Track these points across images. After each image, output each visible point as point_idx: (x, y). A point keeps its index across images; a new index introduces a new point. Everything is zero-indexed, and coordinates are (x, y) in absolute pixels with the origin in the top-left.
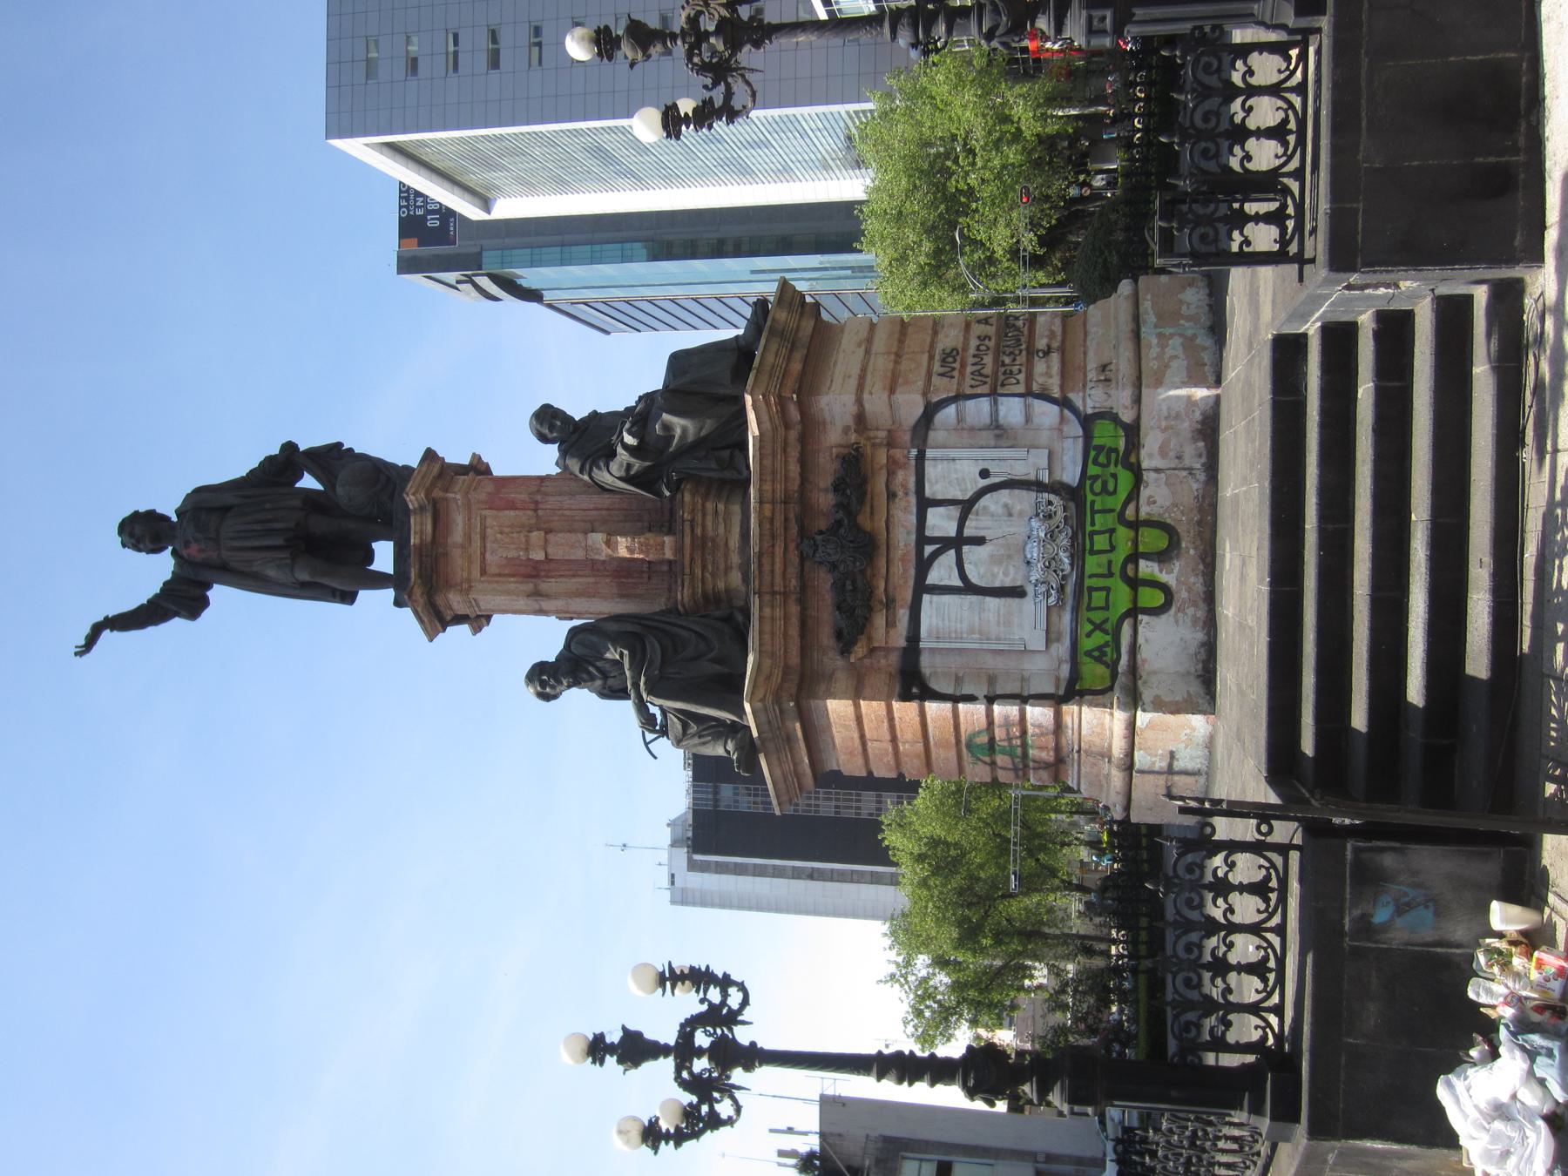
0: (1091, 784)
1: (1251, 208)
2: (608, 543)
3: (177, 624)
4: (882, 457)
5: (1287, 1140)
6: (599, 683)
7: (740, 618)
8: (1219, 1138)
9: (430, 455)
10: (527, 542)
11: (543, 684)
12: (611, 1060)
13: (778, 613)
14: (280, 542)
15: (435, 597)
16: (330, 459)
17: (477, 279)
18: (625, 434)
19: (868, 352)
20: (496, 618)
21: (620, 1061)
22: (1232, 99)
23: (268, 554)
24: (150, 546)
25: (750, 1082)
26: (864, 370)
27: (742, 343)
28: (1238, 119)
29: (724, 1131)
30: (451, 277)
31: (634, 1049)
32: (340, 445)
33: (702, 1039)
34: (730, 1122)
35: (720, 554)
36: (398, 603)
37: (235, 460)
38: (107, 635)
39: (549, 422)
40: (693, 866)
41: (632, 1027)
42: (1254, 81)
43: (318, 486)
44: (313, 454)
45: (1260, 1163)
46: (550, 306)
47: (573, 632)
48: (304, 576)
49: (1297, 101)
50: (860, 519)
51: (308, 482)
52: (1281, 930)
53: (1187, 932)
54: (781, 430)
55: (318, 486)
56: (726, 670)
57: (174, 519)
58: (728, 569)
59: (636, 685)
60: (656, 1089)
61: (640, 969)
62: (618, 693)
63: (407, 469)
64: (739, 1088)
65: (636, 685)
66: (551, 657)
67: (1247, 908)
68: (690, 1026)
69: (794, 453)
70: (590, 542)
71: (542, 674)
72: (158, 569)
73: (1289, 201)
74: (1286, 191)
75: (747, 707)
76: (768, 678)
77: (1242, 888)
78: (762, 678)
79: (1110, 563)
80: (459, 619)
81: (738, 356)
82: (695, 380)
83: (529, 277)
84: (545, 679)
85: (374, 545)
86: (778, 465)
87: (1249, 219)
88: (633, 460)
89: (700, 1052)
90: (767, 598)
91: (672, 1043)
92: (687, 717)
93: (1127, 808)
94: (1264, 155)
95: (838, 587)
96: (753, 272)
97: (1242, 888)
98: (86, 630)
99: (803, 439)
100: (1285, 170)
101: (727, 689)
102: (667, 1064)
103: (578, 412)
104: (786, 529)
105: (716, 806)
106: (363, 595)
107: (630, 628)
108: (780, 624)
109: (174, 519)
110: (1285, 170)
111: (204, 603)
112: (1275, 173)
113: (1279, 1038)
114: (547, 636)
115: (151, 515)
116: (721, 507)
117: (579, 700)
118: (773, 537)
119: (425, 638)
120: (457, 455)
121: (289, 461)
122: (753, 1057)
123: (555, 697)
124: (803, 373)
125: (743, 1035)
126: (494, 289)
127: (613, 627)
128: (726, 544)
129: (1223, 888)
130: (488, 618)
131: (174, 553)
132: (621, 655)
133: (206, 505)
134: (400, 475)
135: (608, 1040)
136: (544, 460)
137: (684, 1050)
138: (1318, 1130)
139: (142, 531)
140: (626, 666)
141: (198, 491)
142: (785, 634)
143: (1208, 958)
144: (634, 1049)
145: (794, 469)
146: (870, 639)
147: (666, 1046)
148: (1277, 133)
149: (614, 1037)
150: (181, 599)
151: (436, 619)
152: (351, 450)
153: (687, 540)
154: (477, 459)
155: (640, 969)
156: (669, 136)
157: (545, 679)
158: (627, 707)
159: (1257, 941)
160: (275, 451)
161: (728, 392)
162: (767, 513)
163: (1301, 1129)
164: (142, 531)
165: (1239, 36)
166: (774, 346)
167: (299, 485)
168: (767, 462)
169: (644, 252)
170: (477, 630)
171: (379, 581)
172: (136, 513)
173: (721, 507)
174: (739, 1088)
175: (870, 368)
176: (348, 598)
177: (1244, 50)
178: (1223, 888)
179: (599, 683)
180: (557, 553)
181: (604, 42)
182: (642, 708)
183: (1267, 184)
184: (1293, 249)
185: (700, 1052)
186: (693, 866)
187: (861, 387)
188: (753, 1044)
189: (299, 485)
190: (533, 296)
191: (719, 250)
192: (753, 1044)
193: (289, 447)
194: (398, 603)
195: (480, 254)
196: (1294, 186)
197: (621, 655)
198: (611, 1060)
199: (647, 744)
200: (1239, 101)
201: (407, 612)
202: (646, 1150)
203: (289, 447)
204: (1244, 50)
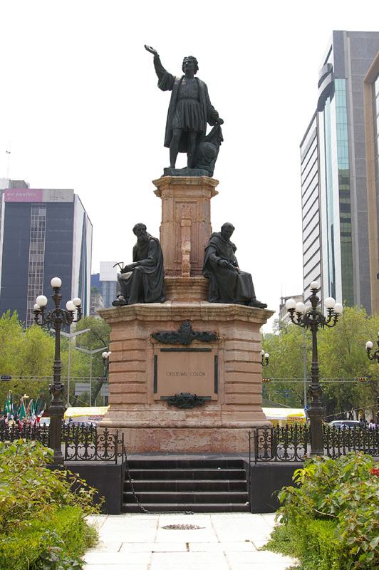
3: (156, 79)
6: (140, 248)
15: (167, 185)
16: (217, 137)
17: (330, 75)
19: (249, 341)
23: (183, 120)
26: (243, 340)
30: (331, 61)
32: (223, 141)
35: (185, 291)
36: (165, 169)
37: (217, 100)
38: (153, 56)
39: (228, 230)
43: (207, 134)
48: (175, 134)
50: (195, 340)
51: (209, 129)
52: (76, 460)
54: (223, 314)
55: (207, 134)
58: (178, 294)
59: (139, 264)
67: (81, 451)
69: (217, 319)
72: (177, 72)
74: (272, 457)
77: (86, 450)
79: (117, 432)
83: (331, 105)
84: (140, 230)
85: (186, 154)
95: (173, 333)
96: (332, 226)
97: (86, 450)
106: (168, 150)
112: (276, 455)
114: (154, 231)
115: (197, 68)
117: (134, 240)
119: (154, 179)
121: (216, 120)
127: (160, 256)
128: (186, 293)
129: (86, 446)
133: (201, 92)
134: (211, 174)
136: (216, 228)
139: (191, 65)
140: (146, 260)
146: (157, 343)
150: (165, 81)
157: (140, 230)
158: (129, 260)
160: (221, 116)
164: (191, 65)
165: (309, 447)
169: (343, 168)
171: (173, 159)
176: (167, 145)
177: (305, 447)
178: (86, 446)
180: (183, 230)
184: (259, 460)
190: (321, 106)
193: (222, 122)
194: (165, 169)
195: (344, 78)
196: (273, 459)
203: (222, 122)
204: (305, 447)
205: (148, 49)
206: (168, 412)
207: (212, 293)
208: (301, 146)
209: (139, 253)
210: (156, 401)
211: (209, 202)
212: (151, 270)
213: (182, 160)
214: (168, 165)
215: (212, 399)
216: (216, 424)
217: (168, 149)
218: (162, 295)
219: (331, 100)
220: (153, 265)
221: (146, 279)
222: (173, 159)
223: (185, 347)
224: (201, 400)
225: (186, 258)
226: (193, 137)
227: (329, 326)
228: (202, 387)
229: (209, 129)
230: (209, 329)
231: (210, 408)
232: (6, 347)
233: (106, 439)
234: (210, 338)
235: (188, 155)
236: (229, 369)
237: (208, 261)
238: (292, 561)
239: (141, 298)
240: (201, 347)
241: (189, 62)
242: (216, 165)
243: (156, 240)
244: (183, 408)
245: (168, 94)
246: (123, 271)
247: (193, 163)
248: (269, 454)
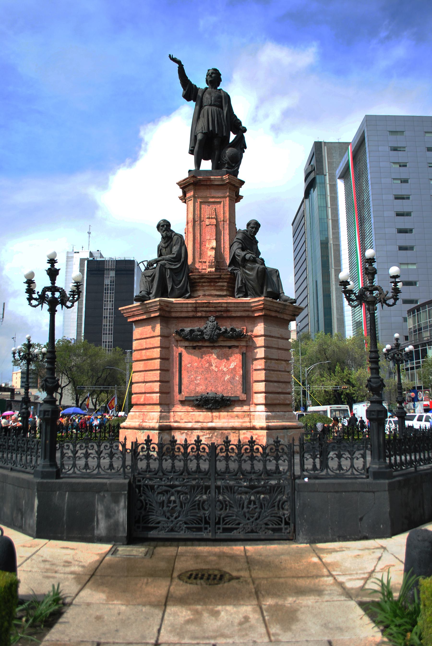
0: (132, 416)
1: (317, 460)
2: (212, 248)
4: (243, 344)
5: (34, 476)
6: (164, 245)
7: (187, 295)
8: (31, 456)
9: (242, 183)
10: (212, 218)
11: (163, 226)
12: (49, 266)
13: (190, 309)
14: (211, 128)
15: (193, 185)
16: (241, 145)
18: (250, 254)
19: (279, 338)
20: (185, 205)
21: (49, 269)
22: (350, 453)
24: (209, 80)
25: (44, 311)
27: (281, 295)
28: (343, 456)
29: (27, 302)
31: (53, 273)
32: (246, 148)
33: (57, 295)
34: (30, 304)
39: (255, 226)
40: (82, 260)
41: (60, 272)
42: (355, 460)
43: (231, 141)
44: (243, 138)
45: (23, 469)
46: (303, 202)
47: (181, 236)
49: (349, 473)
51: (232, 137)
53: (97, 446)
55: (231, 141)
56: (169, 290)
57: (218, 88)
60: (42, 282)
61: (55, 254)
62: (160, 255)
63: (237, 177)
64: (42, 307)
65: (163, 260)
66: (172, 228)
68: (63, 293)
69: (244, 314)
70: (212, 241)
71: (166, 225)
73: (319, 472)
75: (158, 299)
76: (167, 306)
77: (227, 465)
78: (167, 304)
80: (185, 193)
81: (276, 294)
82: (267, 280)
84: (164, 227)
85: (210, 161)
86: (240, 308)
87: (314, 459)
88: (241, 257)
89: (53, 294)
90: (194, 305)
91: (56, 285)
92: (153, 277)
93: (124, 428)
94: (333, 464)
97: (227, 465)
98: (178, 58)
99: (249, 317)
100: (329, 470)
101: (163, 292)
102: (49, 284)
103: (257, 237)
104: (218, 311)
105: (106, 269)
106: (192, 158)
107: (183, 256)
108: (185, 309)
109: (218, 88)
110: (329, 470)
111: (188, 99)
112: (327, 467)
113: (65, 473)
114: (179, 226)
116: (225, 288)
117: (158, 237)
118: (215, 307)
119: (178, 182)
120: (242, 191)
121: (240, 130)
122: (52, 312)
123: (158, 230)
124: (271, 316)
125: (59, 307)
126: (309, 179)
130: (185, 202)
131: (206, 88)
132: (174, 254)
133: (224, 101)
135: (55, 264)
136: (241, 225)
137: (53, 289)
138: (40, 485)
142: (182, 312)
143: (90, 451)
144: (53, 273)
145: (239, 314)
146: (181, 341)
147: (55, 283)
148: (340, 467)
149: (57, 266)
150: (190, 92)
151: (185, 186)
152: (244, 152)
153: (214, 277)
154: (242, 197)
155: (55, 254)
156: (340, 282)
157: (164, 227)
158: (154, 256)
159: (95, 467)
160: (243, 125)
161: (265, 291)
162: (223, 305)
163: (39, 480)
166: (280, 306)
167: (231, 133)
168: (241, 305)
170: (181, 198)
171: (198, 164)
172: (220, 75)
173: (225, 288)
174: (42, 307)
175: (273, 339)
176: (191, 152)
179: (164, 245)
181: (371, 261)
182: (156, 261)
183: (324, 465)
185: (53, 294)
186: (82, 260)
188: (56, 311)
190: (307, 194)
192: (56, 311)
193: (245, 130)
197: (174, 254)
198: (49, 266)
199: (142, 262)
200: (350, 456)
201: (186, 175)
202: (25, 280)
203: (245, 130)
206: (193, 413)
208: (293, 224)
209: (164, 251)
212: (175, 265)
214: (193, 167)
215: (241, 399)
216: (245, 425)
219: (314, 191)
220: (177, 259)
223: (212, 345)
224: (228, 400)
226: (216, 142)
227: (389, 305)
229: (232, 137)
233: (148, 449)
237: (234, 255)
238: (379, 637)
241: (212, 73)
242: (240, 170)
244: (210, 410)
247: (217, 166)
248: (318, 466)
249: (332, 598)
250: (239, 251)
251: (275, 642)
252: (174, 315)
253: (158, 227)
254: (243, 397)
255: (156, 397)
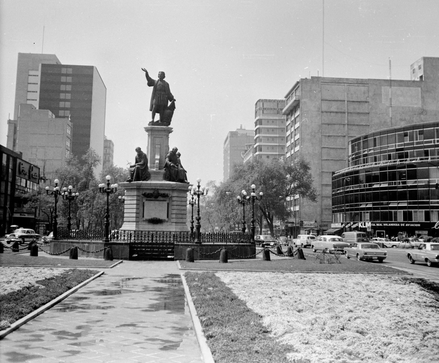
3: (147, 82)
16: (173, 107)
31: (199, 187)
37: (173, 91)
51: (169, 103)
62: (137, 162)
84: (139, 150)
95: (151, 194)
114: (144, 151)
117: (136, 154)
121: (172, 98)
136: (171, 150)
139: (162, 75)
141: (168, 84)
144: (199, 187)
150: (151, 82)
157: (139, 150)
160: (174, 98)
164: (162, 75)
171: (153, 117)
187: (177, 197)
189: (169, 101)
191: (5, 187)
203: (175, 100)
205: (143, 70)
207: (168, 177)
210: (144, 221)
211: (168, 138)
213: (157, 117)
217: (151, 112)
218: (147, 178)
221: (140, 172)
222: (153, 117)
225: (157, 161)
228: (163, 216)
229: (169, 103)
230: (166, 192)
231: (165, 224)
232: (290, 237)
234: (165, 196)
235: (160, 115)
236: (131, 328)
239: (138, 179)
240: (162, 199)
242: (172, 119)
243: (145, 155)
245: (152, 88)
246: (131, 167)
249: (405, 183)
250: (168, 162)
251: (391, 75)
252: (141, 188)
253: (136, 150)
254: (167, 219)
255: (134, 219)
